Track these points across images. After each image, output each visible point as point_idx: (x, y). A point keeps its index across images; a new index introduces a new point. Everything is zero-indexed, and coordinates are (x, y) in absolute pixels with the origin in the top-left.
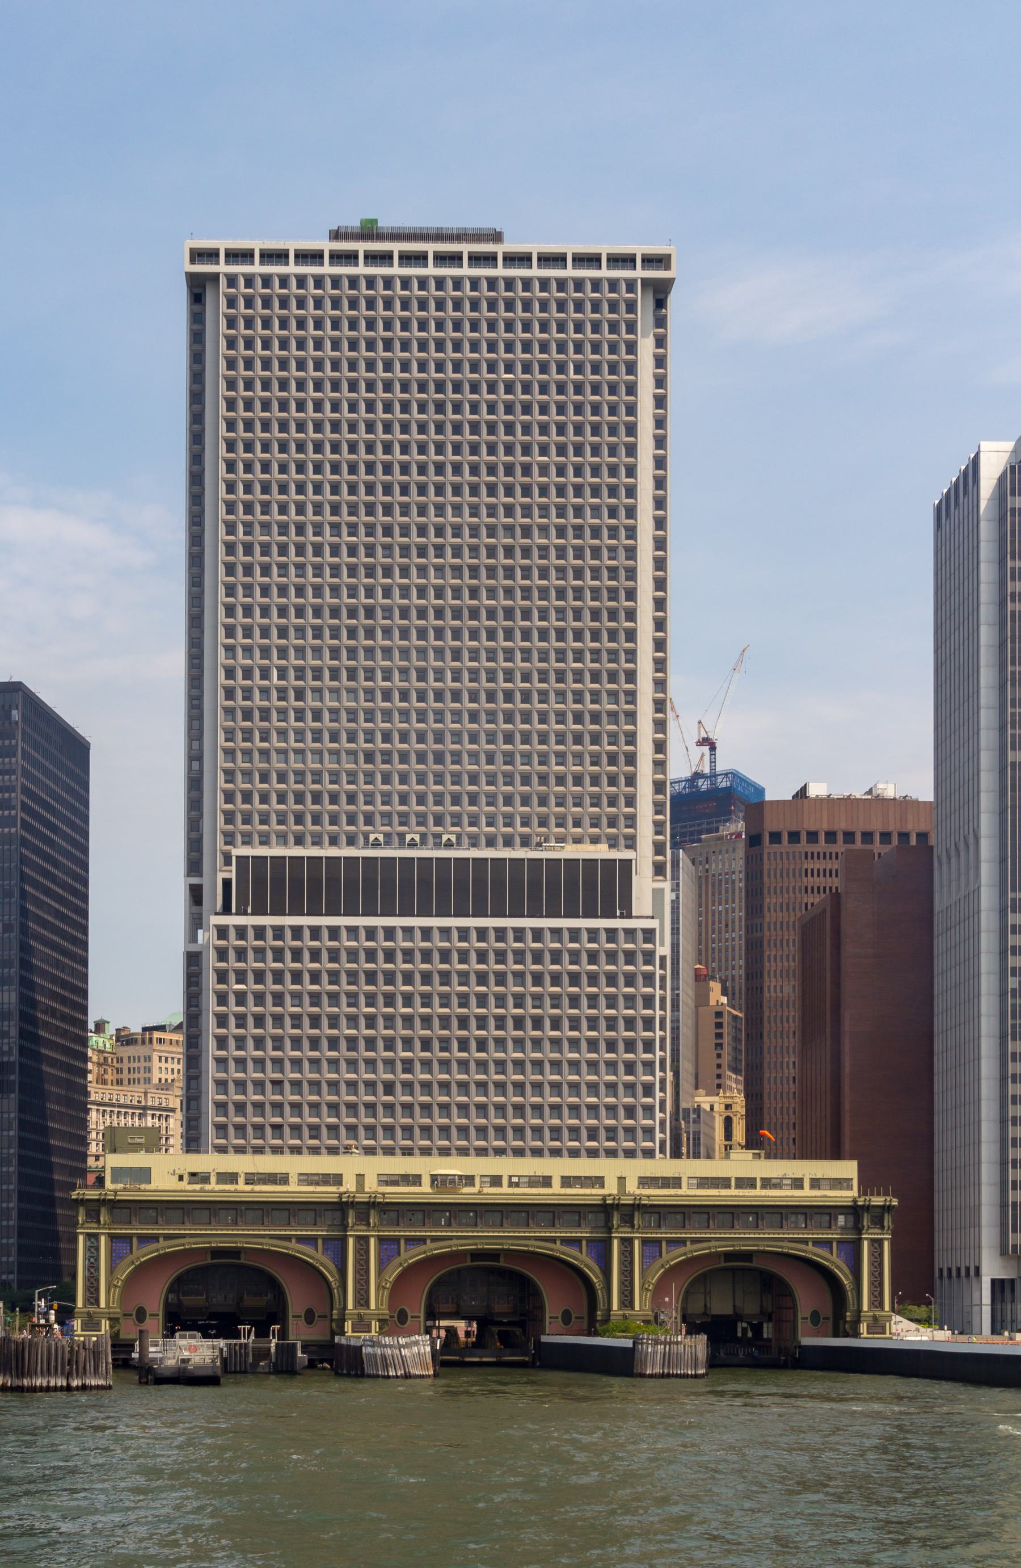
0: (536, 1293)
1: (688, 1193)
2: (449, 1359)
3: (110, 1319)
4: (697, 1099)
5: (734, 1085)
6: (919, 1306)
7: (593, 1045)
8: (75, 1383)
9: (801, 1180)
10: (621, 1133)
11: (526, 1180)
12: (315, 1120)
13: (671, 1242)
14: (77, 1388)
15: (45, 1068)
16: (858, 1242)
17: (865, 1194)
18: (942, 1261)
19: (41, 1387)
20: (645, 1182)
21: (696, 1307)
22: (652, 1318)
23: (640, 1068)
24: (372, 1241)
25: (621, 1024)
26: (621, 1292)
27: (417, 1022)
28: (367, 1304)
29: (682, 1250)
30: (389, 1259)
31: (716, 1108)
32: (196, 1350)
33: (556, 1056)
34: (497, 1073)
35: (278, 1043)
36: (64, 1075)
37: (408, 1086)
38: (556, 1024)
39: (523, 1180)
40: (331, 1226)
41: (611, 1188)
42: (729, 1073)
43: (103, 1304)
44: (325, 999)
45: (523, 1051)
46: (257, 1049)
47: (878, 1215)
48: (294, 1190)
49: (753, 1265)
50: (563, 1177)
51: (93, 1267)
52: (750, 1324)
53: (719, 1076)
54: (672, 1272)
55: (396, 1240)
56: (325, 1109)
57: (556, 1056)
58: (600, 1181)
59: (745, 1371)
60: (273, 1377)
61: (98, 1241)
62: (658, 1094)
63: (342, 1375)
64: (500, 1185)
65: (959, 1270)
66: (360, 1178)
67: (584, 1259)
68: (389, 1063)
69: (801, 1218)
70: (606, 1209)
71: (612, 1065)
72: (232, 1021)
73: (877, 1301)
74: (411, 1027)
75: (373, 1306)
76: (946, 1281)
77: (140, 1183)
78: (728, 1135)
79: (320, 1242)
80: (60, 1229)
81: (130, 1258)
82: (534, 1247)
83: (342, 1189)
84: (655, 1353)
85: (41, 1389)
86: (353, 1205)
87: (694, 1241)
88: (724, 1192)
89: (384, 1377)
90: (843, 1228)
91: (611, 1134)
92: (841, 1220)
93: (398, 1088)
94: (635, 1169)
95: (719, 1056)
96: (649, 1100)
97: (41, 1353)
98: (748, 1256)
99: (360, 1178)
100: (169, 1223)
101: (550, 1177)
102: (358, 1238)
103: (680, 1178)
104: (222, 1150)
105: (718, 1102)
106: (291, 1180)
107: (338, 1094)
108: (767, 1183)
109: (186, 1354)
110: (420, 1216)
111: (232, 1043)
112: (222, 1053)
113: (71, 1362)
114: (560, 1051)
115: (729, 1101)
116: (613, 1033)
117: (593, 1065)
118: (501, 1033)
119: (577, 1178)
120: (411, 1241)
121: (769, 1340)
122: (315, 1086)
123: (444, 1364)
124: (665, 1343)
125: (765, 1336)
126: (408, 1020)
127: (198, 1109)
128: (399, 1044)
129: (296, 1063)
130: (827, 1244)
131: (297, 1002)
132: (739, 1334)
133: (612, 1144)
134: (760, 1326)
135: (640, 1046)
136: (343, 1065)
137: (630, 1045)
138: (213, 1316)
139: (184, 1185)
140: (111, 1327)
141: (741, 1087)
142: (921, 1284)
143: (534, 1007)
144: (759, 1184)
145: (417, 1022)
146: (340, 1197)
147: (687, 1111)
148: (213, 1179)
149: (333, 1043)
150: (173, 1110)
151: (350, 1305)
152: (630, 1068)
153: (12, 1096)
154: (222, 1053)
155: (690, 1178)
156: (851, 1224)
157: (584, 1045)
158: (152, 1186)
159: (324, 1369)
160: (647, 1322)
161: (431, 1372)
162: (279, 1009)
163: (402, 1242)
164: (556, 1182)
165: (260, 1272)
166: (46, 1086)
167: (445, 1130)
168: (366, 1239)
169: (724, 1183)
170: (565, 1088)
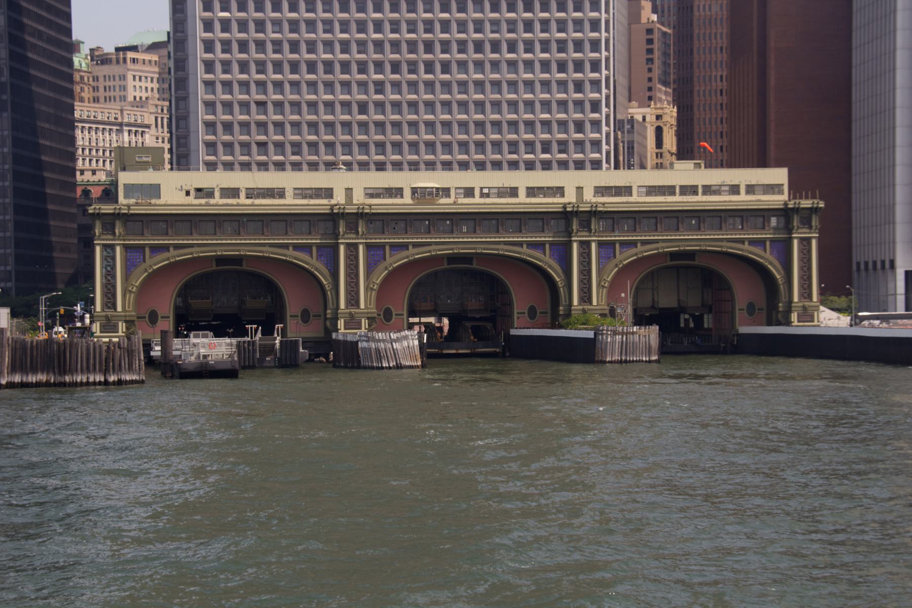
0: (505, 292)
1: (638, 200)
2: (434, 352)
3: (126, 322)
4: (630, 111)
5: (664, 97)
6: (839, 296)
7: (545, 66)
8: (112, 378)
9: (738, 186)
10: (571, 146)
11: (496, 191)
12: (296, 138)
13: (624, 244)
14: (114, 383)
15: (35, 88)
16: (789, 241)
17: (795, 198)
18: (859, 255)
19: (114, 381)
20: (601, 191)
21: (646, 301)
22: (607, 312)
23: (588, 86)
24: (361, 247)
25: (571, 46)
26: (581, 290)
27: (387, 47)
28: (357, 304)
29: (634, 250)
30: (376, 263)
31: (648, 119)
32: (214, 348)
33: (512, 76)
34: (459, 93)
35: (261, 67)
36: (51, 95)
37: (380, 105)
38: (512, 47)
39: (492, 191)
40: (324, 235)
41: (570, 197)
42: (659, 86)
43: (119, 308)
44: (303, 26)
45: (483, 73)
46: (242, 72)
47: (806, 216)
48: (291, 203)
49: (696, 263)
50: (528, 188)
51: (109, 275)
52: (692, 315)
53: (650, 89)
54: (625, 270)
55: (382, 246)
56: (305, 127)
57: (512, 76)
58: (560, 191)
59: (693, 356)
60: (277, 371)
61: (114, 251)
62: (604, 110)
63: (340, 367)
64: (473, 196)
65: (875, 263)
66: (349, 191)
67: (547, 261)
68: (363, 85)
69: (738, 220)
70: (566, 216)
71: (562, 84)
72: (218, 47)
73: (806, 293)
74: (382, 52)
75: (362, 306)
76: (863, 273)
77: (151, 198)
78: (659, 143)
79: (314, 249)
80: (54, 239)
81: (144, 266)
82: (503, 250)
83: (333, 202)
84: (613, 342)
85: (82, 384)
86: (343, 215)
87: (644, 243)
88: (670, 199)
89: (378, 368)
90: (775, 229)
91: (562, 147)
92: (774, 221)
93: (371, 107)
94: (589, 179)
95: (650, 70)
96: (596, 115)
97: (81, 352)
98: (691, 255)
99: (349, 191)
100: (177, 234)
101: (517, 188)
103: (630, 187)
104: (211, 166)
105: (649, 112)
106: (287, 194)
107: (316, 113)
108: (707, 190)
109: (203, 351)
110: (402, 225)
111: (218, 67)
112: (210, 76)
113: (107, 360)
114: (516, 72)
115: (659, 112)
116: (563, 55)
117: (546, 84)
118: (462, 56)
119: (540, 189)
120: (396, 247)
121: (710, 330)
122: (296, 106)
123: (430, 356)
124: (622, 334)
125: (706, 326)
126: (379, 45)
127: (187, 127)
128: (371, 68)
129: (278, 85)
130: (761, 243)
131: (277, 29)
132: (682, 325)
133: (564, 156)
134: (701, 316)
135: (588, 66)
136: (321, 87)
137: (579, 66)
138: (217, 317)
139: (191, 200)
140: (127, 328)
141: (670, 99)
142: (845, 277)
143: (492, 32)
144: (700, 190)
145: (387, 47)
146: (332, 209)
147: (622, 122)
148: (217, 194)
149: (312, 67)
150: (148, 127)
151: (342, 305)
152: (579, 86)
153: (5, 114)
154: (210, 76)
155: (643, 184)
156: (782, 225)
157: (537, 66)
158: (162, 201)
159: (321, 362)
160: (603, 315)
161: (419, 363)
162: (261, 35)
163: (387, 248)
164: (522, 193)
165: (260, 277)
166: (36, 106)
167: (414, 145)
168: (356, 246)
169: (669, 190)
170: (521, 106)
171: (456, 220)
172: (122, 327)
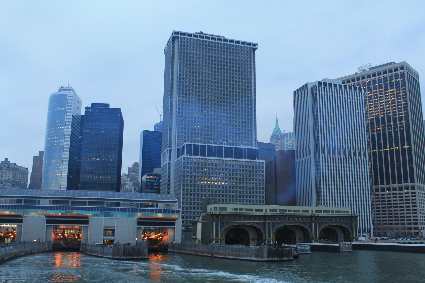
48: (254, 212)
102: (315, 223)
148: (239, 210)
169: (320, 211)
171: (289, 217)
172: (220, 242)
